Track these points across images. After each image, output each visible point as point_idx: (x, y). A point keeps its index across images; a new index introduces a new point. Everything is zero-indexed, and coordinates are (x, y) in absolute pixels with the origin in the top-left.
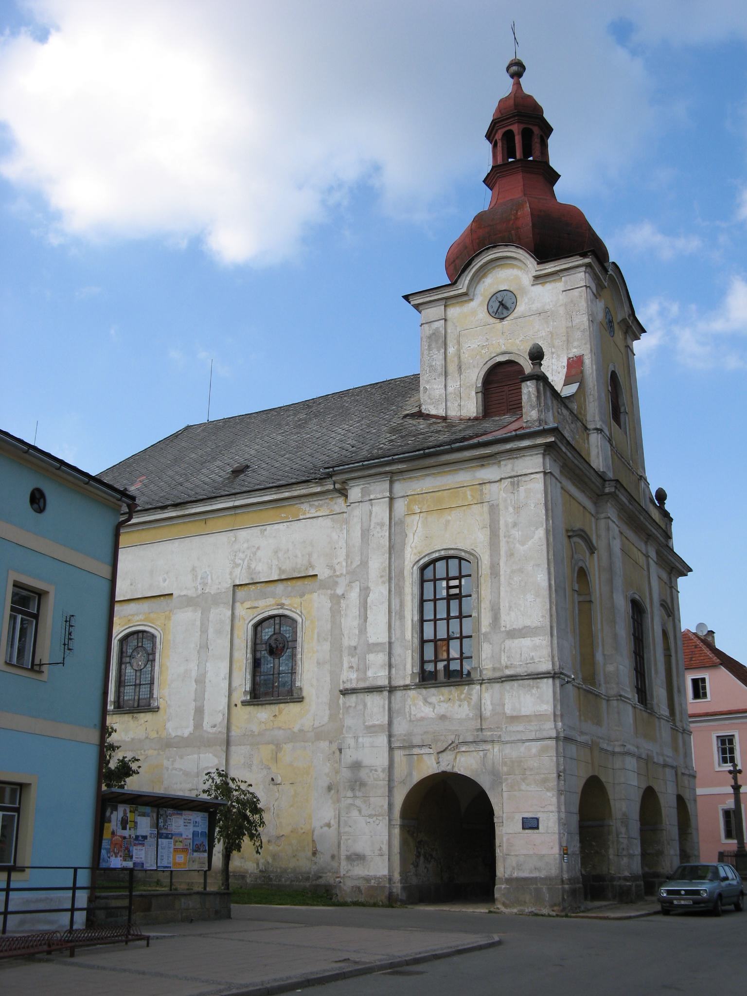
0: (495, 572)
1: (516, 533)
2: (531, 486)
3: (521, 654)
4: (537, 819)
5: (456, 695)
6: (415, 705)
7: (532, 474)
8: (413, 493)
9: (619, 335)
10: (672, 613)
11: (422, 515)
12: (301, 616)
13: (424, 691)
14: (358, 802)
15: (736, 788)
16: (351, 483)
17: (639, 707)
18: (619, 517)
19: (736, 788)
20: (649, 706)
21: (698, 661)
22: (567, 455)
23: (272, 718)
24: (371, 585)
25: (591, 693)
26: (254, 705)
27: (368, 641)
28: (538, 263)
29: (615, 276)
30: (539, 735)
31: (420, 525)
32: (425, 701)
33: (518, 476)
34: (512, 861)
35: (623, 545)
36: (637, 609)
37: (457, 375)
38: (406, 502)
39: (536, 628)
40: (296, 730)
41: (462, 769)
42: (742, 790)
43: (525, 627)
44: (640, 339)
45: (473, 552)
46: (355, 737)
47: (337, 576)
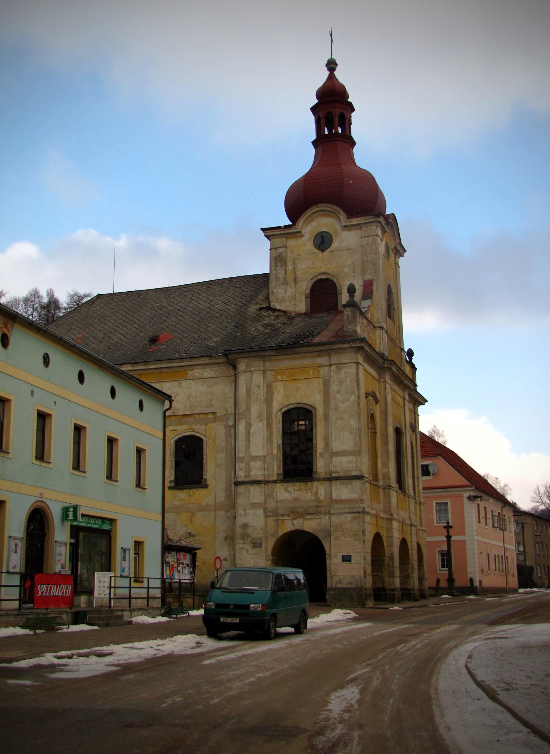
0: (326, 417)
1: (339, 397)
2: (348, 370)
3: (341, 465)
4: (350, 556)
5: (304, 487)
6: (280, 492)
7: (349, 363)
8: (277, 369)
9: (392, 256)
10: (415, 430)
11: (282, 382)
12: (205, 437)
13: (285, 484)
14: (246, 546)
15: (449, 537)
16: (239, 360)
17: (399, 492)
18: (391, 379)
19: (449, 537)
20: (403, 490)
21: (425, 453)
22: (368, 352)
23: (188, 497)
24: (252, 422)
25: (376, 485)
26: (177, 489)
27: (251, 455)
28: (348, 218)
29: (392, 222)
30: (351, 511)
31: (281, 388)
32: (286, 490)
33: (340, 364)
34: (336, 579)
35: (392, 395)
36: (398, 432)
37: (293, 284)
38: (273, 374)
39: (351, 451)
40: (204, 504)
41: (307, 528)
42: (452, 539)
43: (344, 450)
44: (403, 257)
45: (314, 406)
46: (244, 509)
47: (229, 414)
